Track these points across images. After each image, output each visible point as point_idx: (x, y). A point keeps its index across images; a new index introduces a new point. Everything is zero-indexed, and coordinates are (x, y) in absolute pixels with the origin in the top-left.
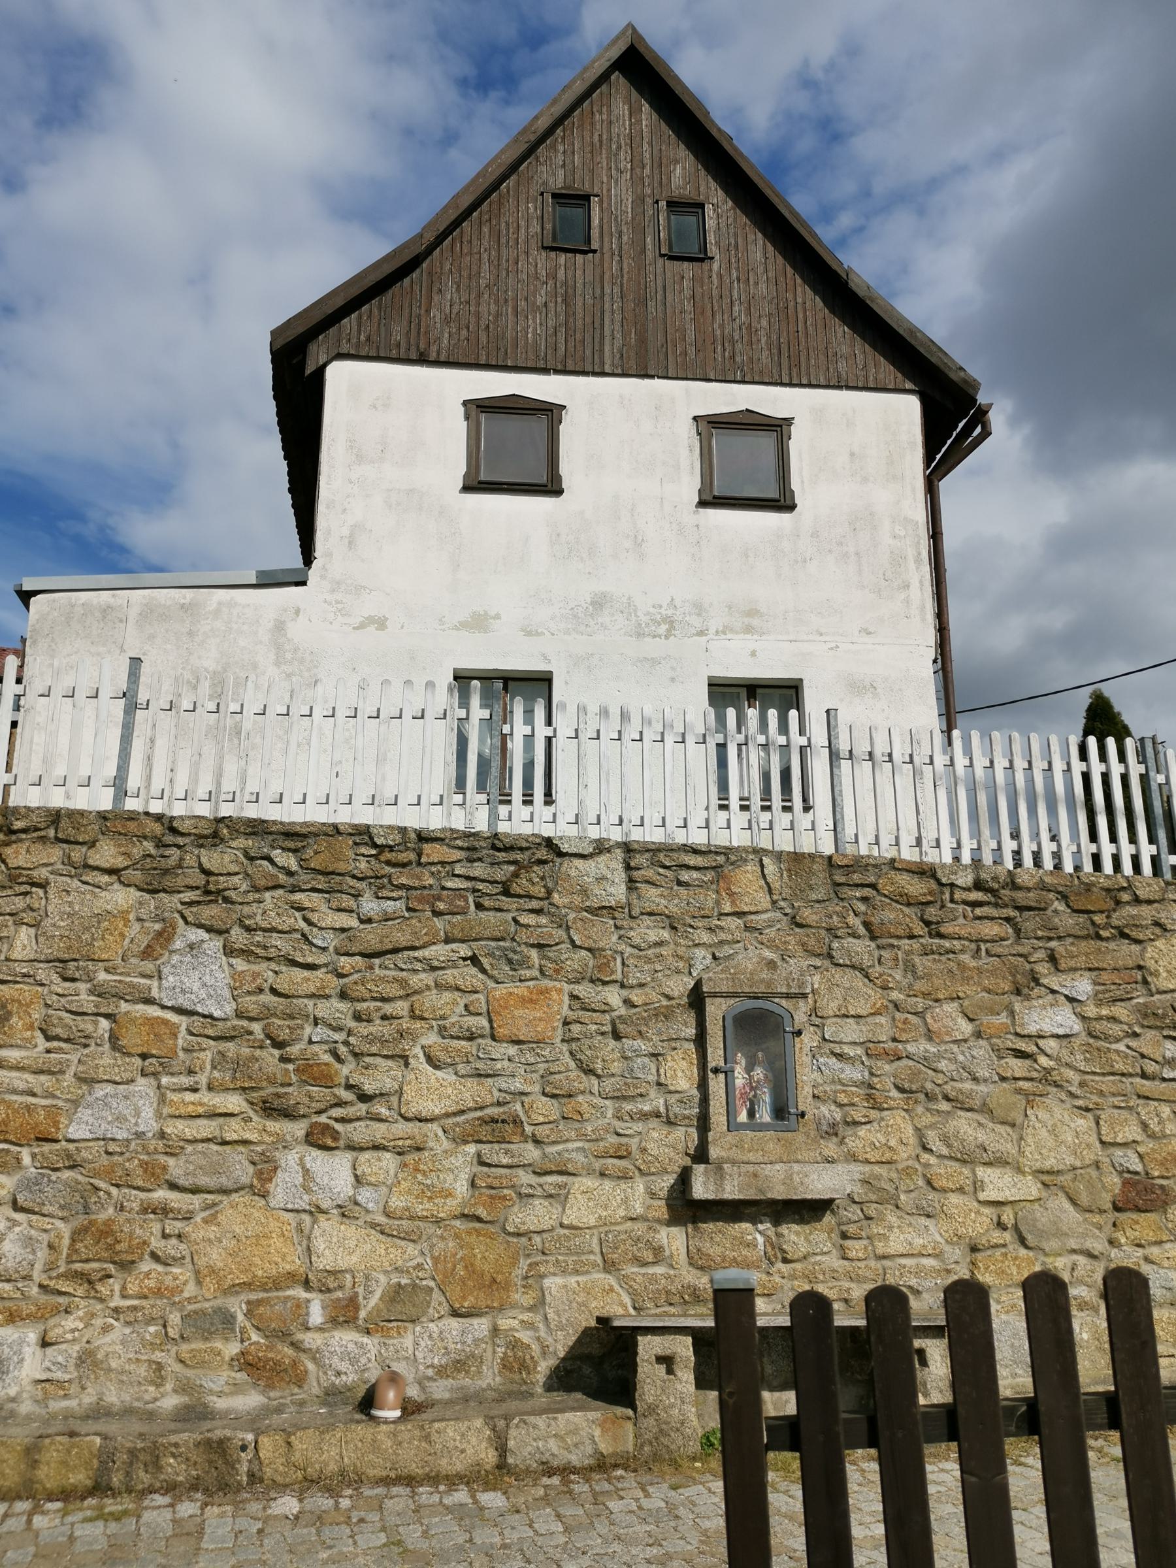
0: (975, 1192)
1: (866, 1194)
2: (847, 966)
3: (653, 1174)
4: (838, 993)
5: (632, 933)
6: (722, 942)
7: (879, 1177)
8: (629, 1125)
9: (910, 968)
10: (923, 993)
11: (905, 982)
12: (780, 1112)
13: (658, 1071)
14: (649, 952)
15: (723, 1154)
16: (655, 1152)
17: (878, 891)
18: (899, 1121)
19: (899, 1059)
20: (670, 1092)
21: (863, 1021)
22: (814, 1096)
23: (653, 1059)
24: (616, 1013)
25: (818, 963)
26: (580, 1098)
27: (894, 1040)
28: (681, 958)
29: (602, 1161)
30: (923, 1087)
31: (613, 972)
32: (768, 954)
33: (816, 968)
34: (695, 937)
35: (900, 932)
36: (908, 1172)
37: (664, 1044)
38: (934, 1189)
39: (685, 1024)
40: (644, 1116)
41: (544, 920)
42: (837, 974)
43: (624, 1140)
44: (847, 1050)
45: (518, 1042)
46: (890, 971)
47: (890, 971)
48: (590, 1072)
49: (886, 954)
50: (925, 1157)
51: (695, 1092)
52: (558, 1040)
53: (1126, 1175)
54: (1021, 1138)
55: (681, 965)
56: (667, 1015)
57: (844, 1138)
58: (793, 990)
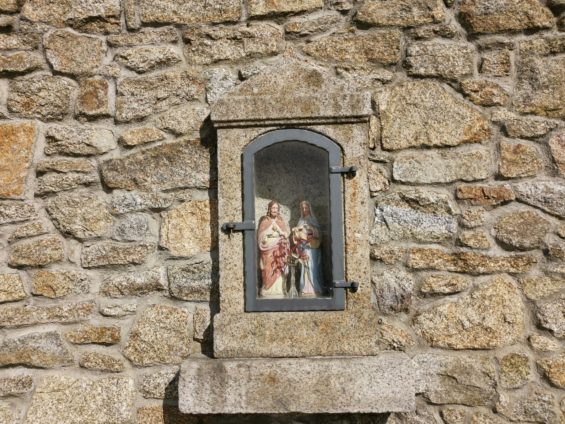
2: (431, 77)
3: (147, 366)
4: (416, 116)
5: (130, 51)
6: (251, 56)
7: (467, 371)
8: (118, 302)
9: (527, 74)
10: (546, 109)
11: (518, 96)
12: (325, 280)
14: (150, 75)
15: (235, 345)
16: (149, 338)
18: (502, 290)
19: (505, 203)
20: (173, 258)
21: (452, 152)
22: (373, 258)
23: (156, 215)
24: (106, 157)
25: (387, 75)
26: (54, 269)
27: (499, 177)
28: (194, 80)
29: (84, 349)
30: (540, 241)
31: (101, 103)
32: (313, 65)
33: (384, 82)
34: (214, 50)
35: (514, 24)
36: (513, 362)
38: (552, 385)
39: (196, 167)
40: (139, 290)
41: (14, 41)
42: (415, 89)
43: (109, 323)
44: (427, 194)
46: (496, 81)
47: (496, 81)
48: (68, 234)
49: (492, 57)
50: (541, 340)
52: (30, 195)
55: (193, 89)
56: (171, 156)
57: (418, 314)
58: (343, 112)
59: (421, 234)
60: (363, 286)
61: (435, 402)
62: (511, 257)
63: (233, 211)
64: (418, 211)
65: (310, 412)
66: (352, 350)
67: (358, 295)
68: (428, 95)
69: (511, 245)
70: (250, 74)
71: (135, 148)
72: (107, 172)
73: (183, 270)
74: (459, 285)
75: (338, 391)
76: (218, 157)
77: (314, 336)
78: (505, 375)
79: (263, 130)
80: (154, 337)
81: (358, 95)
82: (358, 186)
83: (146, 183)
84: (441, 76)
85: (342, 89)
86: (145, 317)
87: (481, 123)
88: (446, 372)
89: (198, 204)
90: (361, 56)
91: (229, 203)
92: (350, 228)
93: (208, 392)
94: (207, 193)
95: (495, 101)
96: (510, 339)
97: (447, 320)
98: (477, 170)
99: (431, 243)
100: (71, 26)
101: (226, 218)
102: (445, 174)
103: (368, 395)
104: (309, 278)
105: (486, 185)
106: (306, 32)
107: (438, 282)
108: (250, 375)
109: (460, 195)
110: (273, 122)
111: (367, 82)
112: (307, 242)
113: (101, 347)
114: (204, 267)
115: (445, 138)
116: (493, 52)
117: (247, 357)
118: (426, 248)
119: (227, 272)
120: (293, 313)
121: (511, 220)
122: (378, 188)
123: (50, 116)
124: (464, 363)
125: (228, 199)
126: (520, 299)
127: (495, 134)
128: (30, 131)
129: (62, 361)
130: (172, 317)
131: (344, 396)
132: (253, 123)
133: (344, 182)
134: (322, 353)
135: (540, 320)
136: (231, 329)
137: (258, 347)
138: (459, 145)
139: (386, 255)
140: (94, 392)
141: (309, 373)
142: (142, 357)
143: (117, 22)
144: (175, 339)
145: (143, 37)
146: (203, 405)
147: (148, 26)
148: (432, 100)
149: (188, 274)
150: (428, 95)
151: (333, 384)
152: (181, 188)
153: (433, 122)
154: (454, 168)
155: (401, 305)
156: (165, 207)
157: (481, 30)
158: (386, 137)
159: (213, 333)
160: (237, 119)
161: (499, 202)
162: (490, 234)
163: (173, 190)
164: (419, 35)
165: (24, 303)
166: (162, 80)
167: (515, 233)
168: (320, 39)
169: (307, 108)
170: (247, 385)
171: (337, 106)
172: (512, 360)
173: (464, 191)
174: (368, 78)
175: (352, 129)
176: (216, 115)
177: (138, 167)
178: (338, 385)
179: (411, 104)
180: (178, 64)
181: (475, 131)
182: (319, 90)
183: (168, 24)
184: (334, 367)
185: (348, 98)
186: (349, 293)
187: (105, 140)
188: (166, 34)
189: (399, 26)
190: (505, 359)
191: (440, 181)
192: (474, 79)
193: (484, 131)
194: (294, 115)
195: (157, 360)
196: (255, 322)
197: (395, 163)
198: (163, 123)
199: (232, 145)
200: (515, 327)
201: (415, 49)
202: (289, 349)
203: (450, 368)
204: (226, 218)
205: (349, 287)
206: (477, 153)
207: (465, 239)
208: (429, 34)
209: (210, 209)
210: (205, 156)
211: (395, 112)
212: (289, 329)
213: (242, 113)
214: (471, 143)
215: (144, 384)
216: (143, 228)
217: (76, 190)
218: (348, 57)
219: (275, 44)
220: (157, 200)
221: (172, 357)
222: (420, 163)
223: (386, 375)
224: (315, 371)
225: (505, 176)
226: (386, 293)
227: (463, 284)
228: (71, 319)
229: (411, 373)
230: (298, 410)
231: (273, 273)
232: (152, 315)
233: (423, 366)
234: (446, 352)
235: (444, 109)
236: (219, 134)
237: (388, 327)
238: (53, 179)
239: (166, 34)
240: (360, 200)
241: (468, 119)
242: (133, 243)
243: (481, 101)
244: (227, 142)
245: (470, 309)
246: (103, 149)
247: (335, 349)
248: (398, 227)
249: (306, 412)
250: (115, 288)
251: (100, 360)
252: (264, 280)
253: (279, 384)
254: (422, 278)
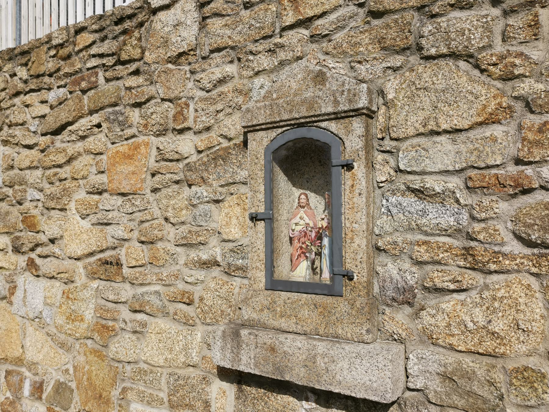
1: (448, 395)
2: (443, 56)
4: (426, 100)
7: (469, 376)
8: (193, 272)
15: (255, 316)
18: (518, 291)
19: (526, 191)
20: (224, 241)
25: (397, 60)
27: (518, 162)
31: (185, 119)
33: (395, 70)
42: (426, 73)
44: (434, 184)
45: (123, 195)
58: (341, 108)
59: (426, 226)
60: (359, 275)
61: (434, 402)
62: (534, 255)
63: (258, 202)
64: (425, 201)
65: (300, 384)
66: (345, 334)
67: (355, 283)
68: (440, 76)
69: (531, 240)
73: (231, 251)
74: (465, 282)
75: (323, 370)
77: (314, 317)
78: (515, 389)
79: (280, 130)
81: (355, 89)
82: (356, 178)
84: (454, 53)
85: (343, 84)
87: (499, 100)
88: (445, 372)
90: (375, 46)
92: (348, 219)
95: (516, 72)
96: (525, 349)
97: (449, 318)
98: (490, 155)
99: (439, 235)
100: (170, 62)
102: (455, 161)
103: (348, 378)
105: (502, 172)
106: (327, 32)
107: (443, 276)
108: (257, 343)
109: (470, 184)
111: (378, 72)
113: (185, 305)
115: (455, 122)
116: (520, 14)
118: (432, 241)
119: (253, 254)
120: (299, 294)
121: (532, 212)
122: (384, 179)
123: (158, 133)
124: (466, 367)
126: (541, 305)
127: (519, 112)
128: (147, 144)
129: (163, 312)
131: (327, 375)
132: (271, 126)
134: (320, 333)
137: (271, 320)
138: (471, 128)
139: (389, 246)
140: (178, 338)
141: (300, 349)
143: (195, 53)
144: (225, 306)
145: (211, 62)
147: (214, 52)
148: (444, 81)
150: (440, 76)
151: (319, 362)
152: (232, 184)
153: (443, 105)
154: (464, 154)
155: (405, 297)
158: (393, 126)
161: (516, 191)
162: (507, 228)
164: (434, 13)
165: (145, 268)
167: (536, 227)
168: (338, 36)
169: (311, 107)
171: (336, 102)
172: (525, 373)
173: (475, 179)
174: (379, 67)
175: (352, 122)
177: (204, 168)
178: (323, 365)
179: (420, 89)
180: (232, 80)
181: (490, 110)
182: (324, 89)
183: (225, 48)
185: (345, 93)
187: (187, 148)
188: (226, 56)
189: (413, 7)
190: (517, 370)
191: (448, 169)
192: (493, 51)
193: (502, 109)
194: (301, 115)
195: (214, 320)
197: (401, 152)
200: (531, 336)
201: (429, 28)
202: (294, 326)
203: (450, 369)
206: (491, 135)
207: (474, 232)
208: (445, 9)
211: (403, 100)
212: (295, 308)
213: (262, 117)
214: (487, 124)
217: (171, 187)
218: (361, 49)
219: (299, 49)
220: (216, 193)
222: (427, 151)
223: (364, 362)
224: (305, 348)
225: (525, 160)
226: (388, 284)
227: (470, 282)
228: (167, 282)
229: (387, 365)
230: (291, 380)
231: (298, 258)
232: (212, 285)
233: (422, 362)
234: (449, 352)
235: (455, 89)
237: (390, 318)
238: (158, 179)
239: (226, 56)
240: (357, 191)
241: (484, 97)
242: (201, 228)
243: (500, 75)
244: (254, 143)
245: (477, 309)
247: (331, 332)
248: (402, 218)
249: (297, 383)
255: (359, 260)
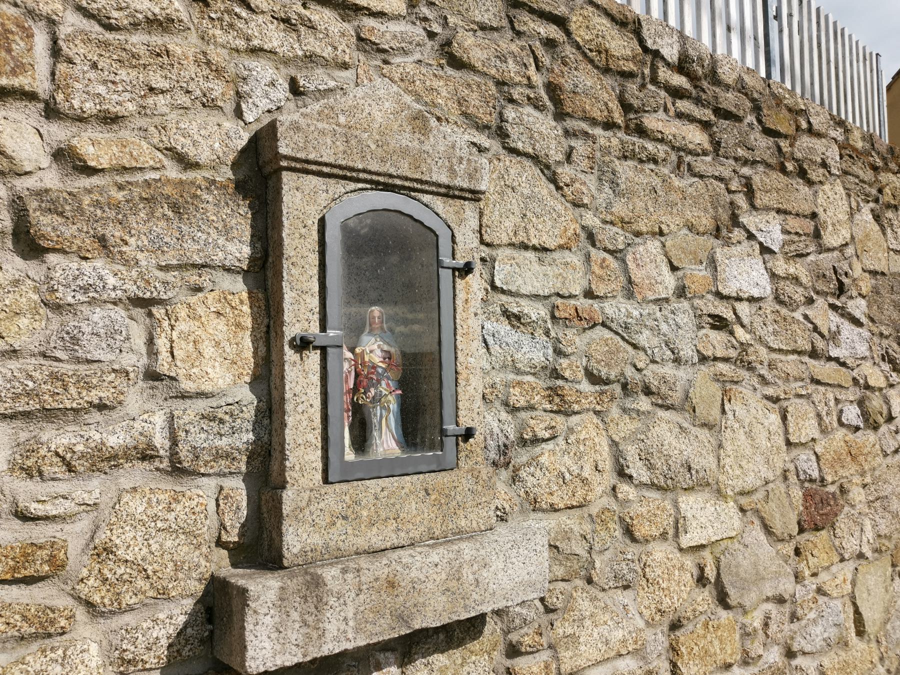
0: (677, 535)
3: (131, 609)
6: (311, 58)
7: (567, 535)
8: (62, 488)
11: (601, 199)
13: (150, 342)
15: (316, 540)
16: (136, 553)
17: (568, 33)
20: (184, 396)
21: (548, 257)
23: (139, 312)
24: (29, 182)
25: (483, 140)
27: (589, 294)
28: (218, 72)
30: (622, 374)
31: (19, 68)
34: (252, 29)
35: (596, 114)
37: (170, 276)
38: (634, 540)
39: (226, 231)
40: (105, 461)
43: (41, 533)
49: (578, 145)
50: (625, 489)
51: (246, 395)
53: (807, 485)
54: (720, 446)
55: (218, 88)
63: (308, 314)
65: (439, 625)
66: (469, 525)
70: (312, 88)
71: (101, 174)
72: (38, 213)
73: (203, 417)
74: (558, 427)
76: (284, 219)
79: (353, 186)
80: (145, 550)
83: (124, 249)
86: (124, 513)
89: (230, 297)
91: (301, 300)
93: (297, 625)
94: (240, 278)
101: (297, 325)
104: (388, 426)
106: (386, 47)
109: (557, 314)
110: (369, 177)
112: (385, 370)
113: (14, 587)
114: (242, 411)
115: (544, 239)
117: (336, 558)
119: (298, 417)
125: (300, 293)
130: (179, 507)
131: (477, 590)
133: (454, 282)
134: (435, 536)
135: (622, 466)
136: (311, 514)
137: (351, 538)
142: (118, 594)
144: (186, 549)
146: (289, 650)
149: (211, 424)
151: (465, 575)
152: (194, 266)
156: (165, 297)
157: (570, 110)
159: (282, 523)
160: (320, 160)
163: (180, 267)
166: (158, 55)
170: (357, 601)
171: (452, 171)
176: (287, 145)
177: (112, 214)
178: (471, 577)
180: (185, 34)
184: (466, 551)
186: (461, 444)
187: (28, 146)
196: (347, 498)
197: (497, 263)
198: (164, 139)
199: (305, 203)
204: (297, 325)
205: (460, 436)
209: (251, 307)
210: (242, 212)
212: (393, 505)
215: (124, 647)
216: (118, 337)
218: (440, 101)
221: (182, 583)
223: (521, 550)
230: (424, 625)
236: (285, 180)
245: (566, 457)
246: (25, 163)
250: (56, 460)
251: (17, 617)
252: (368, 425)
253: (400, 589)
254: (523, 420)
255: (476, 410)
